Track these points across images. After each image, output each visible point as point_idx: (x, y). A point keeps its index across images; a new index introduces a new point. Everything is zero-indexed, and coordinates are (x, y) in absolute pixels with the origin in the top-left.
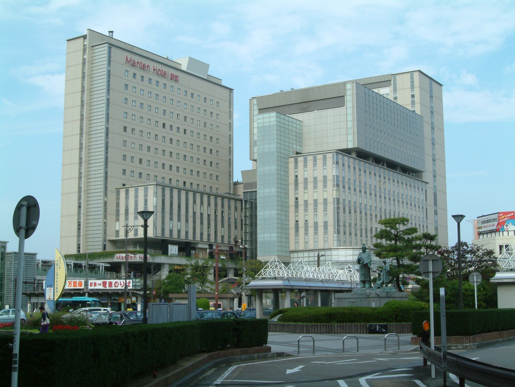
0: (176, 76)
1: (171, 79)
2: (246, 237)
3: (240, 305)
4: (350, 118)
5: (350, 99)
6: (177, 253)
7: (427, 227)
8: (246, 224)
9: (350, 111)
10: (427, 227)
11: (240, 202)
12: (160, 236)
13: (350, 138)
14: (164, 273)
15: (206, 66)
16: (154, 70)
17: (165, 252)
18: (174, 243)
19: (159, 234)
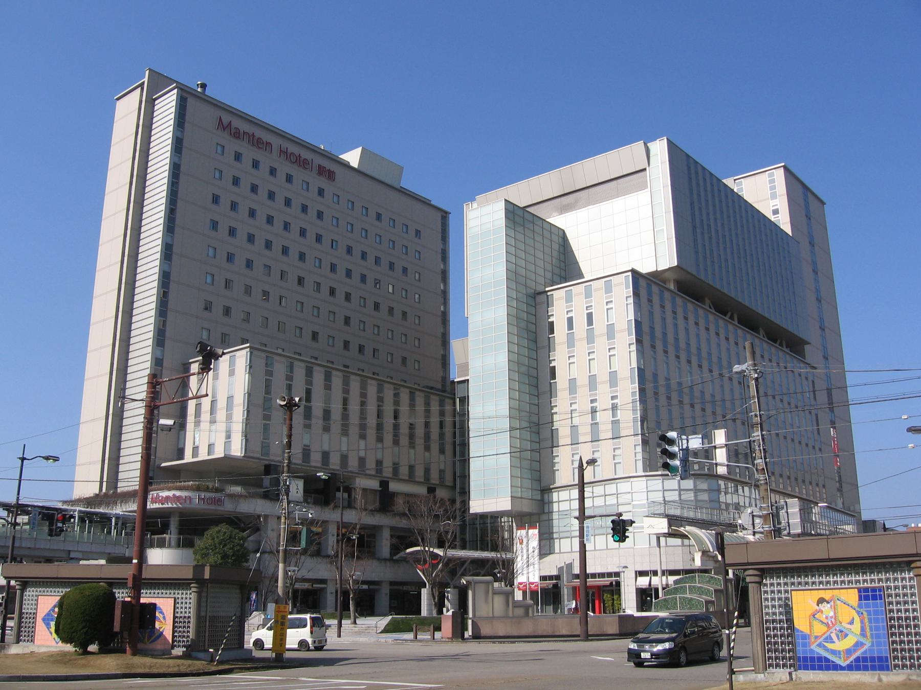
0: (329, 170)
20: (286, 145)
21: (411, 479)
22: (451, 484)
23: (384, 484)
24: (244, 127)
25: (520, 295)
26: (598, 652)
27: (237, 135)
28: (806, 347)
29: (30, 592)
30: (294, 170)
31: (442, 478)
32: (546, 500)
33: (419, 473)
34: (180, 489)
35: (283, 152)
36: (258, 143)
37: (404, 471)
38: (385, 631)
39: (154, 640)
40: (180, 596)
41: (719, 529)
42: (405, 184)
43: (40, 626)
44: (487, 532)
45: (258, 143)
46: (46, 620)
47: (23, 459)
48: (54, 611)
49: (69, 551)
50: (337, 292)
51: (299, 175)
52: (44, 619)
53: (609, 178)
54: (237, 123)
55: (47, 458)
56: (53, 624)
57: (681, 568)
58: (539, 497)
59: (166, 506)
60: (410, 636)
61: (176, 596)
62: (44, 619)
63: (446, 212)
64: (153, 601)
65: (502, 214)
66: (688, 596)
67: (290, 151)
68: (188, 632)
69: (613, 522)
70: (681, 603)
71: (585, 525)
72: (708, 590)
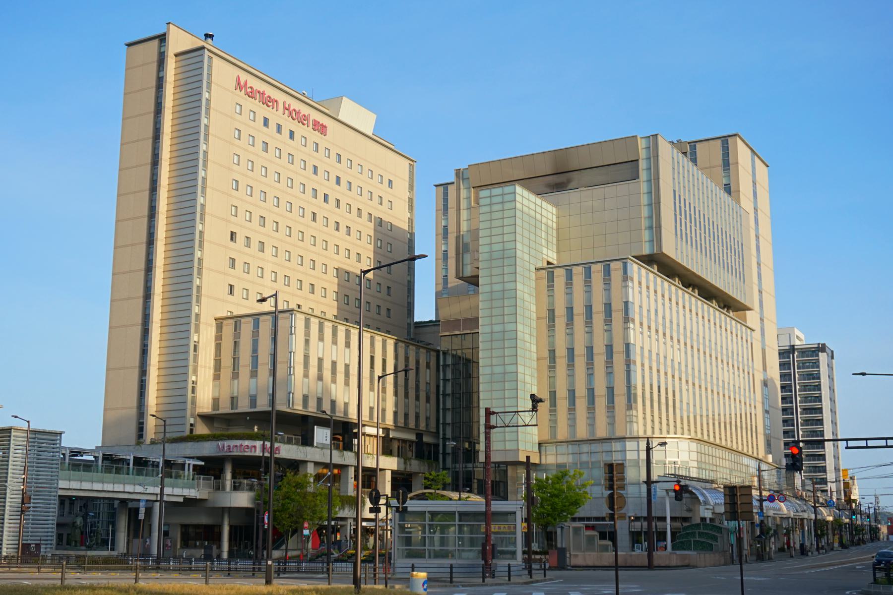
0: (322, 125)
3: (375, 510)
6: (328, 442)
8: (445, 395)
17: (307, 440)
18: (323, 423)
35: (286, 109)
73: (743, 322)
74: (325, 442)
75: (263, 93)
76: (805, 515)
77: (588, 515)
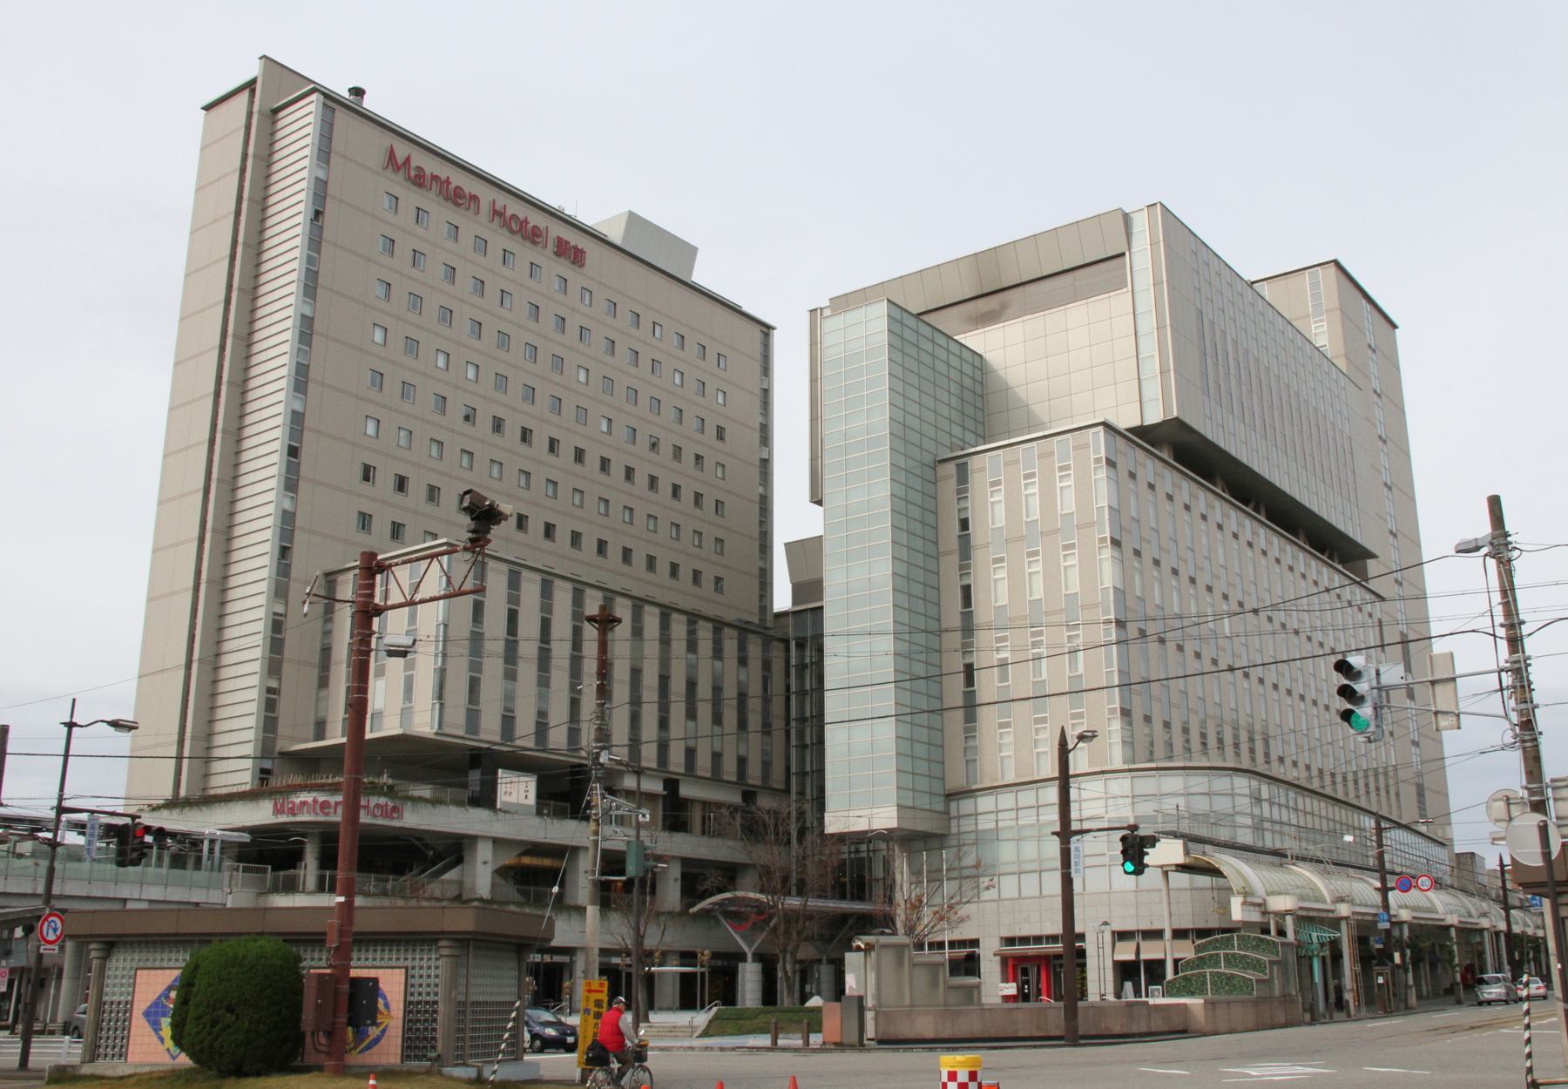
0: (575, 248)
1: (558, 254)
2: (802, 760)
4: (1148, 323)
5: (1144, 258)
7: (1397, 795)
9: (1146, 300)
10: (1397, 795)
11: (781, 646)
12: (497, 739)
13: (1153, 389)
14: (481, 874)
15: (691, 251)
16: (495, 212)
17: (485, 798)
18: (519, 764)
19: (457, 726)
20: (502, 200)
21: (716, 778)
22: (782, 786)
23: (671, 784)
24: (432, 166)
25: (911, 463)
26: (1143, 1062)
27: (419, 180)
28: (1370, 563)
29: (120, 963)
30: (515, 245)
31: (766, 775)
32: (953, 813)
33: (730, 769)
34: (320, 788)
35: (497, 213)
36: (457, 197)
37: (704, 764)
38: (706, 1033)
39: (368, 1048)
40: (417, 963)
41: (87, 1030)
42: (699, 277)
43: (139, 1025)
44: (857, 869)
45: (457, 197)
46: (152, 1015)
47: (71, 725)
48: (167, 997)
49: (125, 901)
50: (587, 457)
51: (526, 254)
52: (147, 1014)
53: (1060, 269)
54: (419, 159)
55: (115, 724)
56: (166, 1022)
57: (1189, 926)
58: (940, 807)
59: (299, 818)
60: (764, 1040)
61: (409, 963)
62: (147, 1014)
63: (769, 327)
64: (372, 973)
65: (883, 324)
66: (1223, 970)
67: (509, 213)
68: (434, 1030)
69: (1123, 839)
70: (1214, 983)
71: (1073, 846)
72: (1258, 961)
73: (1361, 579)
74: (523, 801)
75: (448, 181)
76: (1485, 923)
77: (1036, 932)
